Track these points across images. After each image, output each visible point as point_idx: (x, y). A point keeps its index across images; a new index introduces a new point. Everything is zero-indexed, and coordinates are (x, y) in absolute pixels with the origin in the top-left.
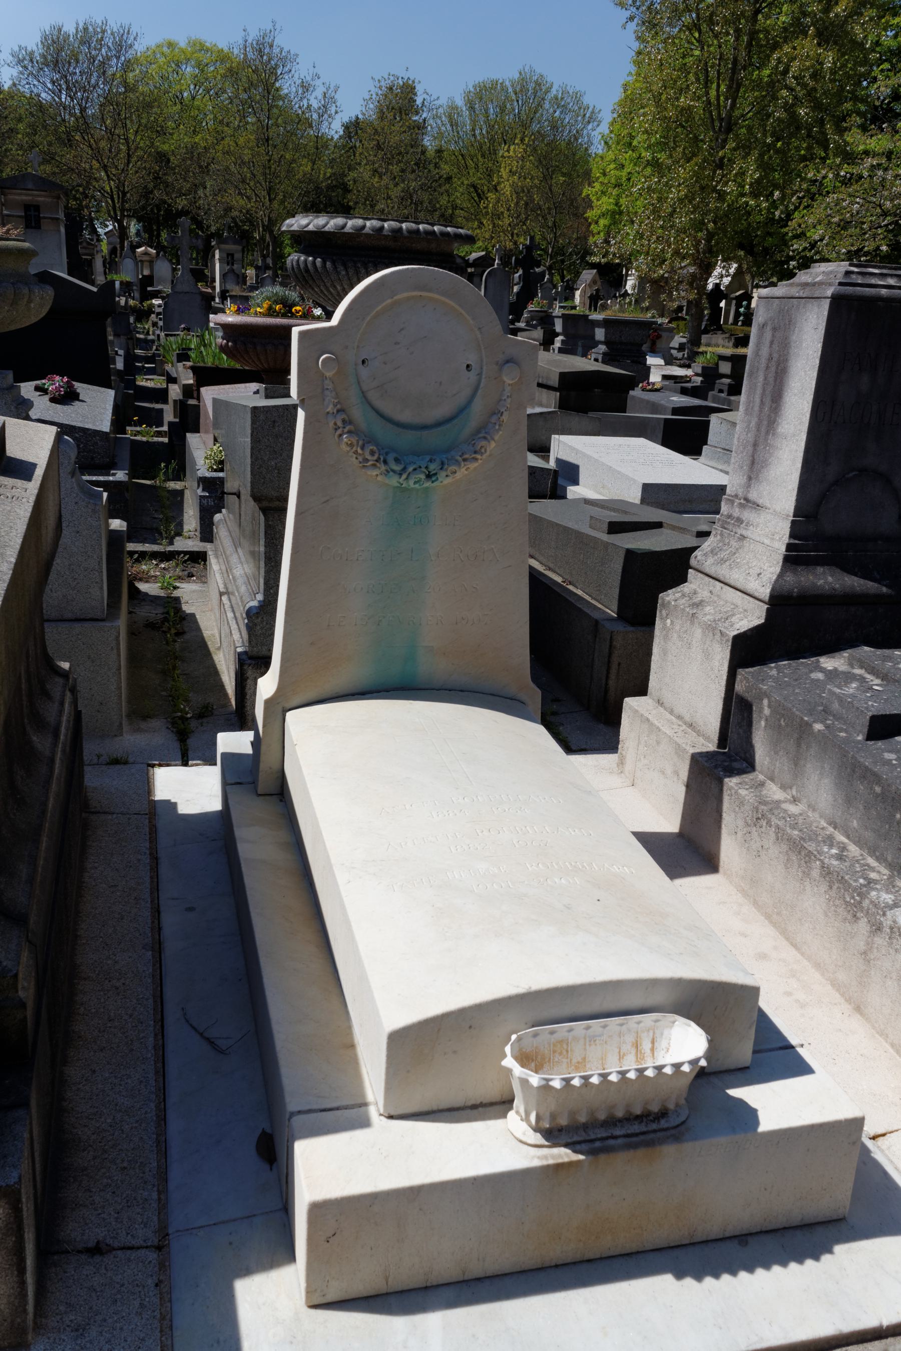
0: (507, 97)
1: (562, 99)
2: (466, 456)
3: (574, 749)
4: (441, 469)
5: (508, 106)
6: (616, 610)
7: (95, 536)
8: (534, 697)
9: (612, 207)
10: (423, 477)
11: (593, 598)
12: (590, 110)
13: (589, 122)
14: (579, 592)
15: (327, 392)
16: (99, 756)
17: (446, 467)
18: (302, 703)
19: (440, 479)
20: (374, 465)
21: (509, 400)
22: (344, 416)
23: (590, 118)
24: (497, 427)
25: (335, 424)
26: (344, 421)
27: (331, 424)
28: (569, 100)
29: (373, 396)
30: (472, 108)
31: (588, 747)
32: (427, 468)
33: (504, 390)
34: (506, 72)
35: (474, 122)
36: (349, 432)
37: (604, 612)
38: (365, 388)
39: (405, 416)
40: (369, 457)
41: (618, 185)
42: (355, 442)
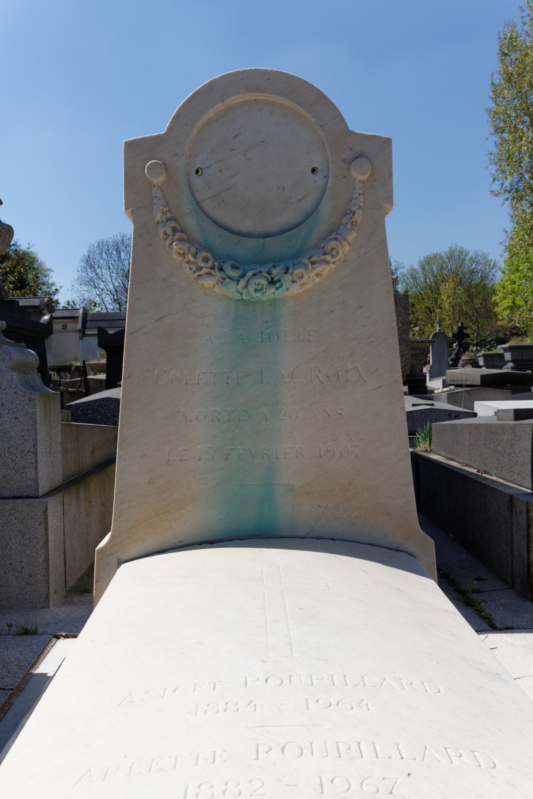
0: (443, 261)
1: (476, 258)
2: (314, 259)
3: (499, 626)
4: (286, 273)
5: (444, 265)
6: (530, 486)
7: (30, 422)
8: (426, 547)
9: (510, 304)
10: (265, 282)
11: (506, 480)
12: (493, 262)
13: (493, 268)
14: (494, 478)
15: (156, 201)
16: (10, 626)
17: (291, 270)
18: (140, 554)
19: (285, 285)
20: (209, 274)
21: (361, 198)
22: (173, 224)
23: (493, 266)
24: (349, 226)
25: (165, 234)
26: (175, 230)
27: (162, 234)
28: (479, 258)
29: (209, 206)
30: (423, 269)
31: (515, 626)
32: (269, 273)
33: (355, 188)
34: (441, 248)
35: (425, 276)
36: (180, 240)
37: (518, 490)
38: (199, 198)
39: (246, 225)
40: (202, 264)
41: (513, 292)
42: (186, 249)
